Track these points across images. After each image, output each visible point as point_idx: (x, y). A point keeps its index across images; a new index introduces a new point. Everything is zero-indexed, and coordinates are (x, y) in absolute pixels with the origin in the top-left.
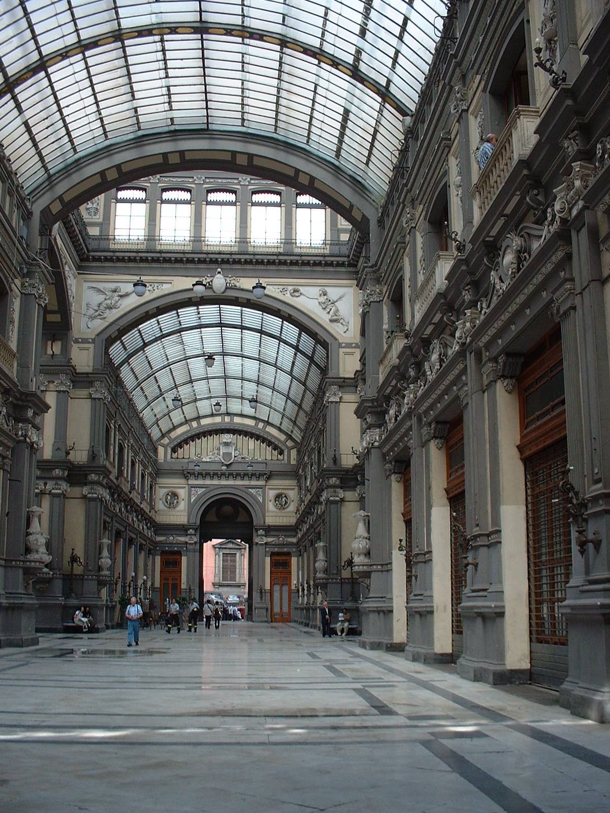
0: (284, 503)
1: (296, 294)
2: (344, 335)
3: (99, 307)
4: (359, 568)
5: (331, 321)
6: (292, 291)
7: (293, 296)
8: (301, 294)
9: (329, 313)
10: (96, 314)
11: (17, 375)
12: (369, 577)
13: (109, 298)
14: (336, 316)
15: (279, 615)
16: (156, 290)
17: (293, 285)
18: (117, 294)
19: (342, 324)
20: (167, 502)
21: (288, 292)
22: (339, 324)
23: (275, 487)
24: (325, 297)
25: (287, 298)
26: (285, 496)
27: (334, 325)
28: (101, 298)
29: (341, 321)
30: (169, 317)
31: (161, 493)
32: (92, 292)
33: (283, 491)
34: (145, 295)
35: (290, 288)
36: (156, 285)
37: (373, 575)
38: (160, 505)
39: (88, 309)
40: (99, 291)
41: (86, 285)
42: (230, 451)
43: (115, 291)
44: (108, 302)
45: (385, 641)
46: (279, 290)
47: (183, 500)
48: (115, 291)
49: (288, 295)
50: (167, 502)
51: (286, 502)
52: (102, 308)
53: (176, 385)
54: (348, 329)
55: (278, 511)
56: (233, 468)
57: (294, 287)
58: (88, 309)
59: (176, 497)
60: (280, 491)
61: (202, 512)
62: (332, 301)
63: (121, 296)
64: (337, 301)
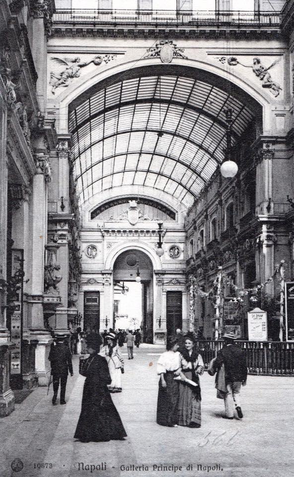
0: (176, 254)
2: (276, 99)
3: (61, 76)
4: (48, 300)
5: (264, 86)
6: (230, 60)
7: (230, 65)
8: (238, 62)
9: (262, 79)
10: (60, 82)
13: (70, 68)
14: (269, 81)
16: (111, 60)
17: (230, 55)
18: (77, 64)
19: (273, 89)
20: (88, 254)
21: (226, 61)
22: (271, 89)
23: (171, 241)
24: (260, 65)
26: (178, 248)
27: (267, 90)
28: (62, 68)
29: (273, 87)
30: (112, 97)
32: (55, 62)
33: (175, 244)
34: (101, 65)
35: (228, 57)
36: (111, 55)
39: (52, 78)
40: (61, 61)
43: (75, 61)
44: (70, 71)
46: (218, 60)
47: (100, 252)
48: (75, 61)
49: (226, 64)
50: (88, 254)
51: (178, 253)
52: (64, 76)
54: (278, 94)
55: (172, 259)
57: (231, 56)
58: (52, 78)
59: (95, 250)
60: (173, 244)
61: (115, 259)
62: (265, 69)
63: (81, 66)
64: (269, 68)
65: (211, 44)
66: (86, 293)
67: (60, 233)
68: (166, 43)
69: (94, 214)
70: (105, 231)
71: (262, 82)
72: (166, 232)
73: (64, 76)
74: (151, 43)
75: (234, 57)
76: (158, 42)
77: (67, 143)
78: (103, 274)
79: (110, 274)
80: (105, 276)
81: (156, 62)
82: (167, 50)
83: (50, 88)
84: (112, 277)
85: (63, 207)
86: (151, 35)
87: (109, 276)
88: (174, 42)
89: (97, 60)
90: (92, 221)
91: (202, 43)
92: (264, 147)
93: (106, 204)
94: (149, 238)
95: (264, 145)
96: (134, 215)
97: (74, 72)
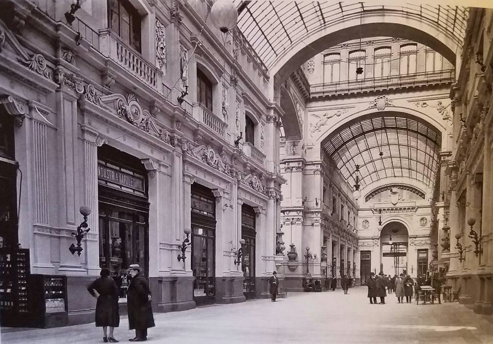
1: (425, 105)
9: (442, 115)
10: (316, 129)
11: (469, 116)
12: (449, 260)
15: (119, 248)
18: (326, 117)
25: (420, 109)
31: (360, 221)
32: (314, 118)
37: (451, 259)
38: (360, 227)
41: (309, 113)
42: (140, 221)
45: (360, 280)
53: (371, 162)
56: (397, 206)
65: (411, 94)
66: (361, 251)
67: (315, 219)
68: (381, 98)
69: (368, 198)
70: (375, 210)
71: (443, 117)
72: (418, 208)
73: (318, 125)
74: (372, 98)
75: (425, 102)
76: (376, 97)
77: (319, 166)
78: (373, 239)
79: (378, 239)
80: (374, 241)
81: (375, 110)
82: (381, 102)
83: (309, 133)
84: (379, 241)
85: (317, 204)
86: (372, 94)
87: (377, 240)
88: (386, 96)
89: (339, 113)
90: (367, 202)
91: (404, 95)
92: (442, 159)
93: (373, 193)
94: (406, 213)
95: (442, 157)
96: (394, 199)
97: (324, 122)
